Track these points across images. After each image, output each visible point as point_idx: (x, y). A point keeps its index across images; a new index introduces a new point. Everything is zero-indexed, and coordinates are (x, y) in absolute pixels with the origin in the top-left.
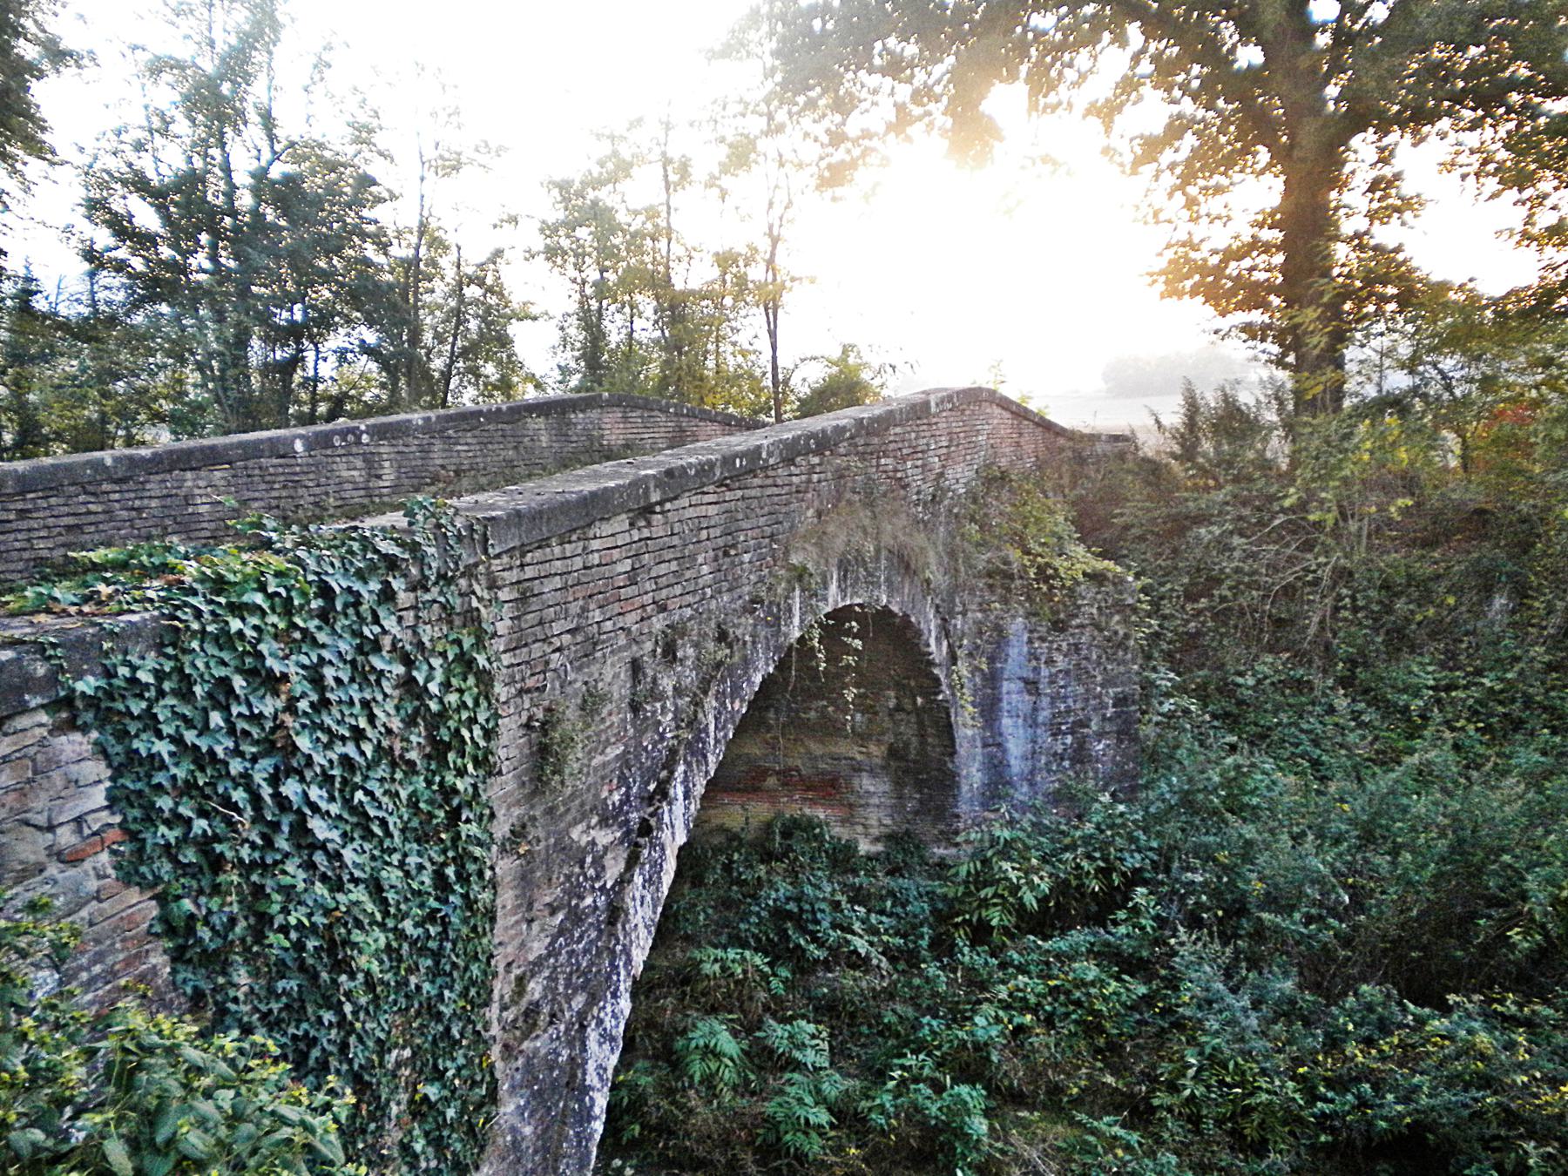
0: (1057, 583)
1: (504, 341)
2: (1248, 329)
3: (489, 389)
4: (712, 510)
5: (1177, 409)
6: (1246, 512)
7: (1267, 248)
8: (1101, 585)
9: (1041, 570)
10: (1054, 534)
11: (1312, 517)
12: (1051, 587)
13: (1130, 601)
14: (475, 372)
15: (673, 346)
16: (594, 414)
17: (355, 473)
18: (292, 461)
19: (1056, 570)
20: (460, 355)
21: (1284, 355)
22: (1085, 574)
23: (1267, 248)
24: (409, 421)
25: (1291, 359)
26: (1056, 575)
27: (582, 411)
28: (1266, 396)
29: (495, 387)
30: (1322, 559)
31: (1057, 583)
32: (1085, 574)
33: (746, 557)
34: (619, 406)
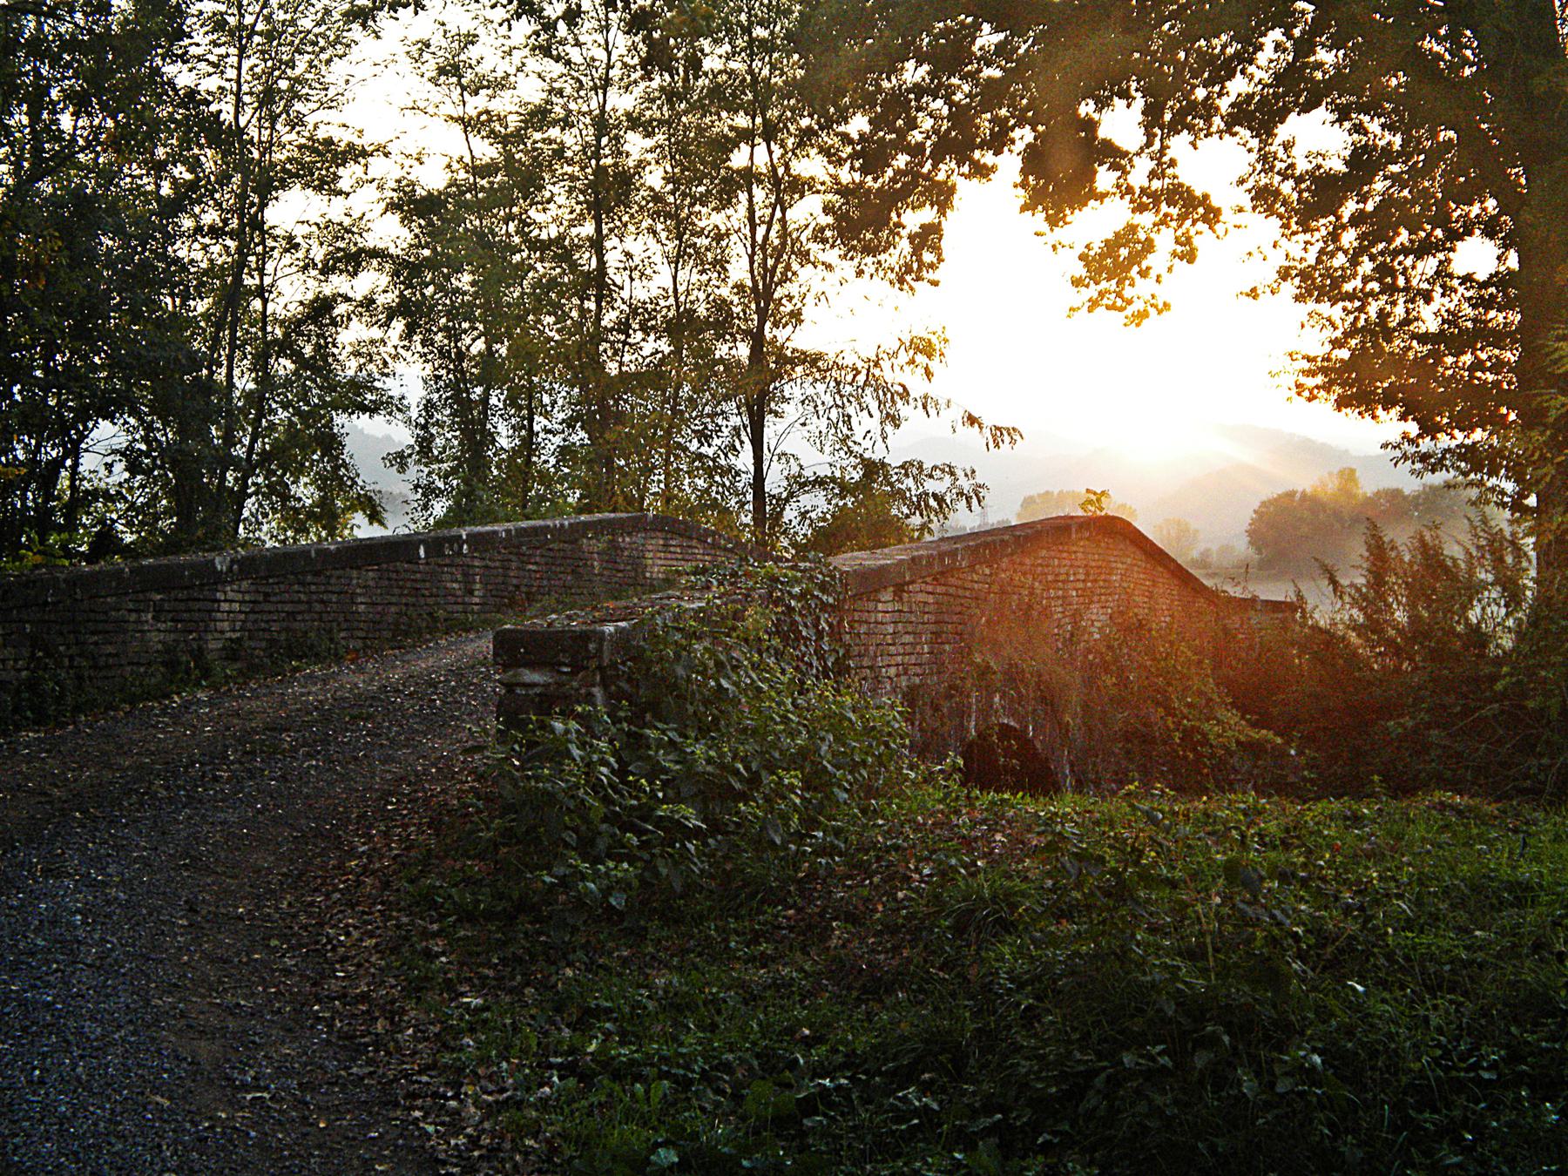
0: (1206, 750)
1: (331, 443)
2: (1469, 454)
3: (296, 519)
4: (931, 599)
5: (1359, 561)
6: (1448, 700)
7: (1498, 338)
8: (1259, 758)
9: (1187, 734)
10: (1200, 693)
11: (1531, 704)
12: (1199, 755)
13: (1291, 779)
14: (279, 492)
15: (600, 457)
16: (639, 538)
17: (455, 585)
18: (414, 567)
19: (1204, 735)
20: (260, 464)
21: (1522, 495)
22: (1239, 743)
23: (1498, 338)
24: (495, 533)
25: (1532, 501)
26: (1205, 742)
27: (629, 534)
28: (1479, 548)
29: (311, 515)
30: (1545, 761)
31: (1206, 750)
32: (1239, 743)
33: (947, 647)
34: (662, 530)
